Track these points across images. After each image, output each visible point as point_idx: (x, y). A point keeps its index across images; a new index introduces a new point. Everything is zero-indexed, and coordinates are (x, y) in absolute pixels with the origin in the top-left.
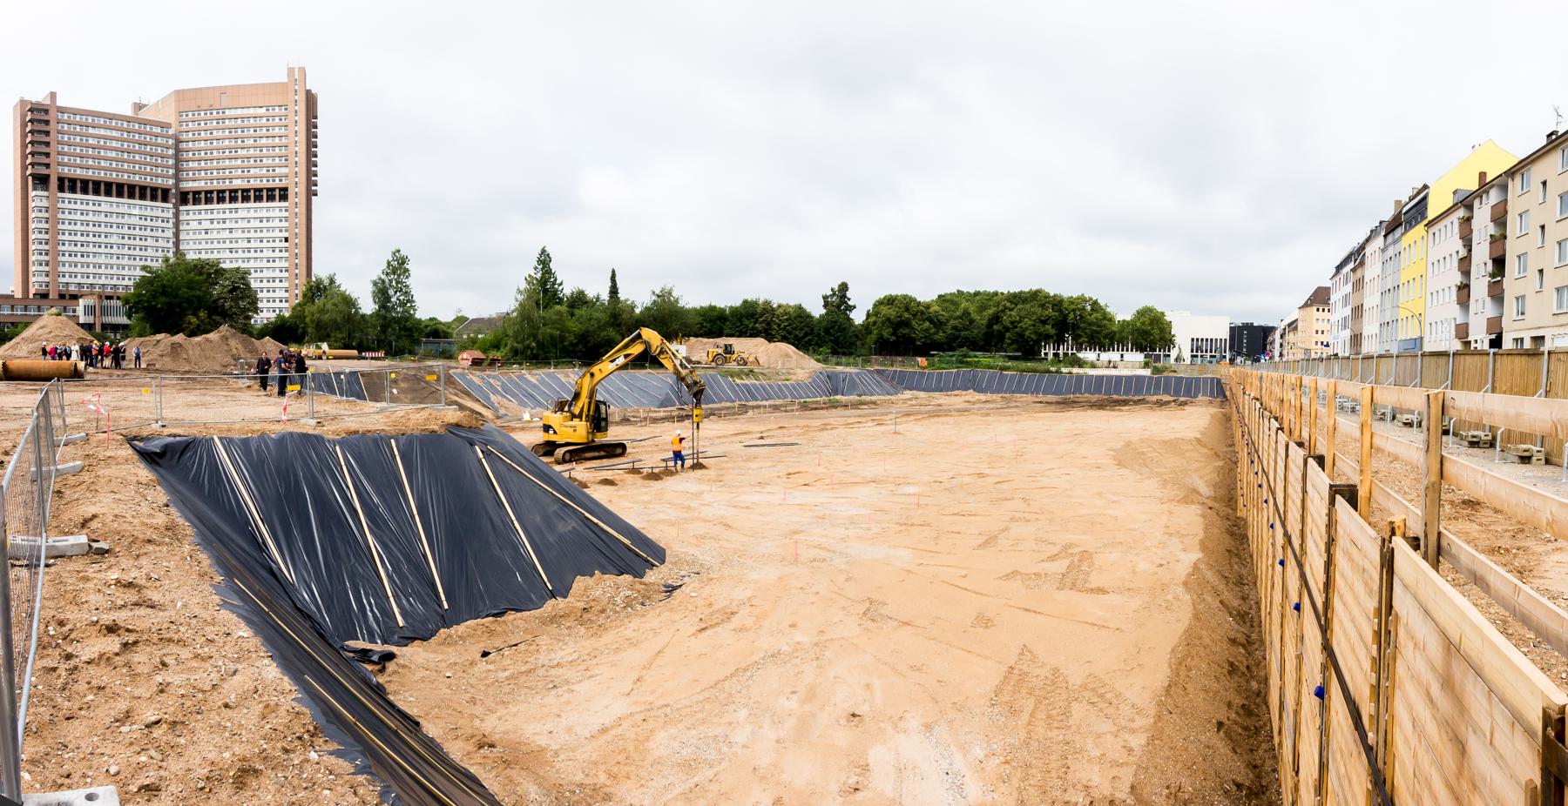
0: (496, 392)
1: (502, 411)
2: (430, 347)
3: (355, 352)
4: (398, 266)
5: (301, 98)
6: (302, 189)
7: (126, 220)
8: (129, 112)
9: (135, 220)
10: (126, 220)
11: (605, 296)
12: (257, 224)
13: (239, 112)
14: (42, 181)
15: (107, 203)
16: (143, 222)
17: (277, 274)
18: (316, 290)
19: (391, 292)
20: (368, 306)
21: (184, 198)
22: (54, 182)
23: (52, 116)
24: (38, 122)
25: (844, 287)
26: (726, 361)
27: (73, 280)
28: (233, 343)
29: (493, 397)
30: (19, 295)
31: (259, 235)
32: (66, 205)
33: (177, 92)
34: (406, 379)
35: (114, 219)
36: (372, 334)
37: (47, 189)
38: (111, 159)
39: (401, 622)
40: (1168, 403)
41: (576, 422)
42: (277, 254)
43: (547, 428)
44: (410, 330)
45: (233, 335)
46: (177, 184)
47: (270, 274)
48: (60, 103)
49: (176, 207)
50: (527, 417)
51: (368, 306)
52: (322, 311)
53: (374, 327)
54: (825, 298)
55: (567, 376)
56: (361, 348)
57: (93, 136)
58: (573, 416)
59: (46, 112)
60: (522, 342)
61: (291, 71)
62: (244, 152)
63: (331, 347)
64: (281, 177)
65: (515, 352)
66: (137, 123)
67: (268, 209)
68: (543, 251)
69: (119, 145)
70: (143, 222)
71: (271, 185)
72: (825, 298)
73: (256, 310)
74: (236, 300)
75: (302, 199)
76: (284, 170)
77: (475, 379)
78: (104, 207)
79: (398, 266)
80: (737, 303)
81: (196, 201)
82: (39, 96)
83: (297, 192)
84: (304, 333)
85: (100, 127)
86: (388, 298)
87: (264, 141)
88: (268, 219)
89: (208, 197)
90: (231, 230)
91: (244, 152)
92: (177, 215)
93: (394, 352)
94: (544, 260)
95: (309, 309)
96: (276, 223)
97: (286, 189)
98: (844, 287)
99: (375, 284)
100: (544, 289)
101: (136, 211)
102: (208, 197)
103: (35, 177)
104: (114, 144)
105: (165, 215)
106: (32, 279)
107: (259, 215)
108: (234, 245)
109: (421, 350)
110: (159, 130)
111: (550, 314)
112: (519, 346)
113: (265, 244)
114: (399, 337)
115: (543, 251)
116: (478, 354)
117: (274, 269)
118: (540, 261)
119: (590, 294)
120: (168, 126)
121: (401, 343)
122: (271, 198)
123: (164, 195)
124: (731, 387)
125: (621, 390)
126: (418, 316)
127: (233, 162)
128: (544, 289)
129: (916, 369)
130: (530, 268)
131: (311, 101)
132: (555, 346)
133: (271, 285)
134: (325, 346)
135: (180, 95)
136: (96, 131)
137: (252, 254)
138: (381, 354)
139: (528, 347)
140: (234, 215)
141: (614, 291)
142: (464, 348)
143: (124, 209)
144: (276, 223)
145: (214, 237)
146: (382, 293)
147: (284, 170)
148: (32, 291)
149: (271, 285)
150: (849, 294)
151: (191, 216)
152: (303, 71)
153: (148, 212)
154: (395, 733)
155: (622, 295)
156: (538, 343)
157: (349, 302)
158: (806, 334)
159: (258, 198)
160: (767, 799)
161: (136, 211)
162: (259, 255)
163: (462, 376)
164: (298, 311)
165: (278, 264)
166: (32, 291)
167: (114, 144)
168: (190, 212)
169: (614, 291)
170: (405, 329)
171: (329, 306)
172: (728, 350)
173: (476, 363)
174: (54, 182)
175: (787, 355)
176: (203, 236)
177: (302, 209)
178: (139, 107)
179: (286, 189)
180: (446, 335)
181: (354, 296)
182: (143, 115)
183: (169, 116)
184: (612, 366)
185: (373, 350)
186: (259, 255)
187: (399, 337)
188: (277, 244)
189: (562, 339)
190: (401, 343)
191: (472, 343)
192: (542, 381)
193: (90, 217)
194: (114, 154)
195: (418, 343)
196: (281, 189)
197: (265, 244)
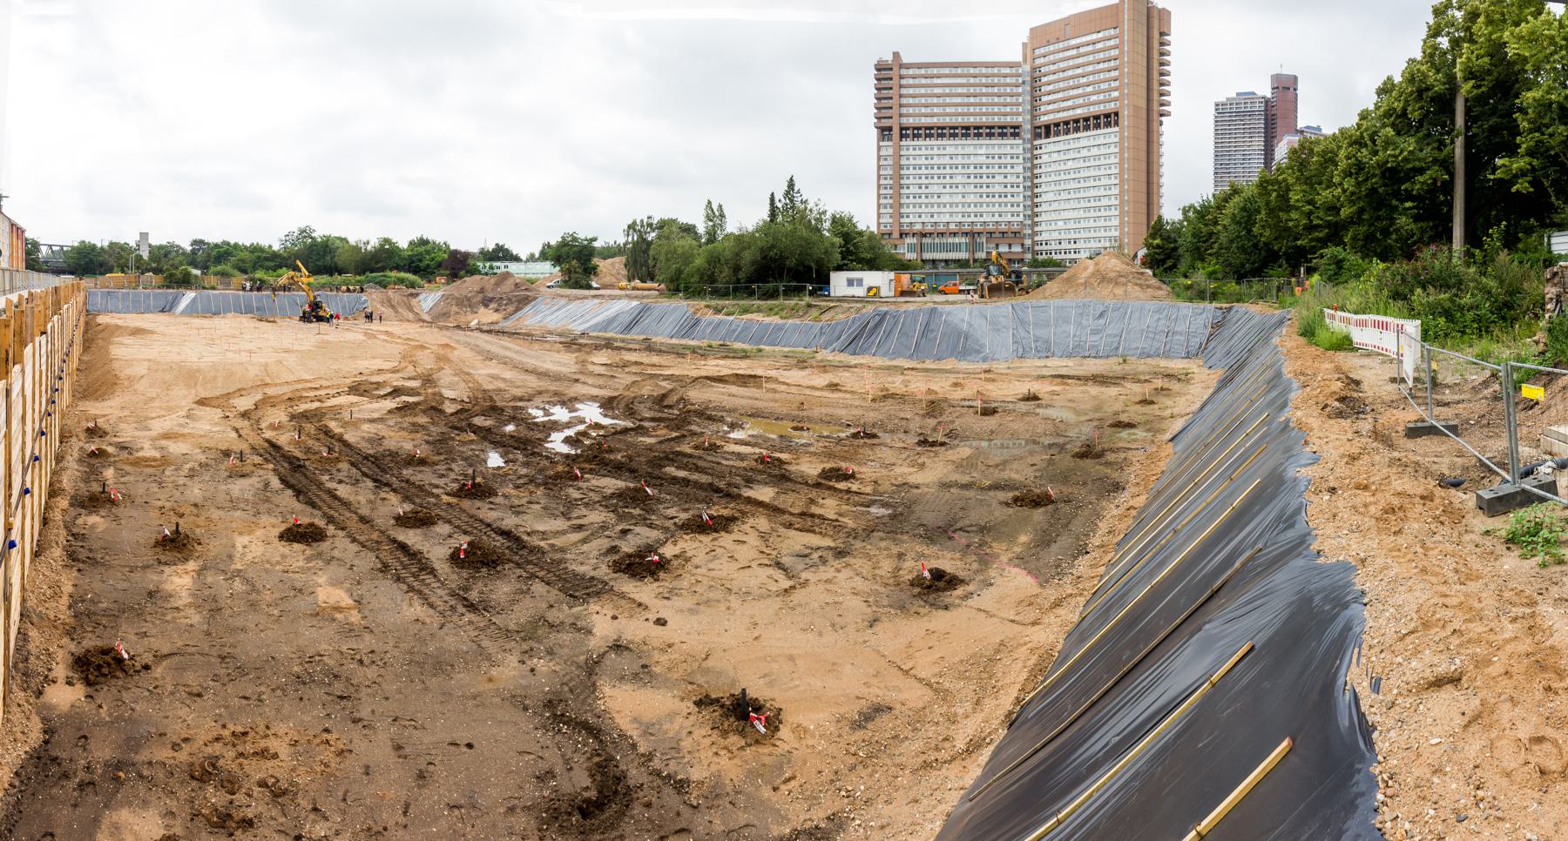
7: (973, 160)
9: (982, 159)
10: (973, 160)
15: (952, 146)
16: (990, 161)
24: (888, 75)
27: (979, 219)
32: (911, 152)
35: (959, 160)
39: (1285, 743)
40: (372, 374)
69: (1013, 80)
70: (990, 161)
78: (950, 150)
80: (218, 240)
89: (929, 132)
102: (929, 132)
105: (1015, 151)
123: (1015, 131)
143: (971, 150)
154: (1059, 822)
160: (513, 760)
168: (1050, 148)
174: (896, 131)
193: (936, 161)
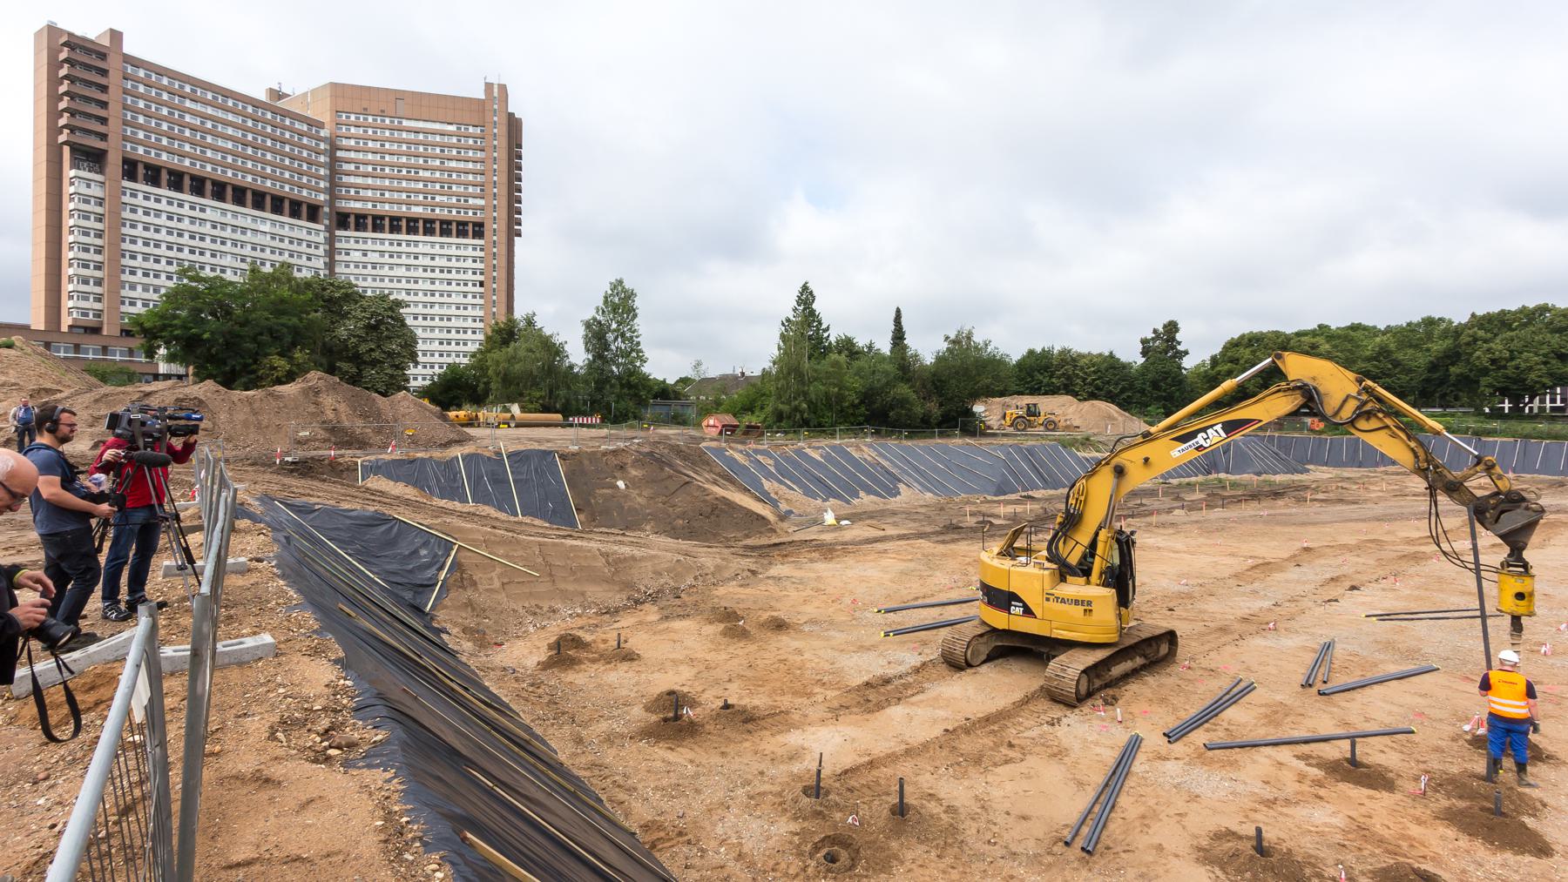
0: (769, 475)
1: (783, 507)
2: (658, 410)
3: (559, 417)
4: (621, 304)
5: (501, 130)
6: (501, 226)
8: (262, 96)
11: (885, 346)
12: (443, 262)
13: (421, 125)
14: (92, 158)
17: (469, 323)
18: (505, 334)
19: (610, 337)
20: (577, 355)
21: (342, 220)
22: (114, 162)
23: (113, 64)
25: (1172, 328)
26: (1030, 425)
28: (328, 401)
29: (767, 485)
30: (39, 323)
31: (445, 275)
33: (334, 86)
34: (638, 463)
36: (583, 393)
37: (101, 172)
38: (225, 151)
41: (1074, 588)
42: (469, 299)
43: (1001, 598)
44: (635, 387)
45: (333, 388)
46: (331, 203)
47: (461, 323)
48: (128, 48)
49: (329, 229)
50: (830, 518)
51: (577, 355)
52: (512, 359)
53: (587, 382)
54: (1144, 342)
55: (858, 448)
56: (567, 411)
57: (194, 113)
58: (1064, 571)
59: (103, 56)
60: (789, 403)
61: (489, 87)
62: (427, 174)
63: (523, 409)
64: (475, 209)
65: (779, 416)
66: (272, 111)
67: (458, 246)
68: (805, 288)
71: (462, 217)
72: (1144, 342)
73: (413, 357)
74: (380, 341)
75: (501, 238)
76: (481, 202)
77: (737, 456)
79: (621, 304)
81: (360, 226)
82: (90, 28)
83: (496, 227)
84: (487, 392)
85: (206, 103)
86: (606, 347)
87: (453, 164)
88: (458, 258)
90: (408, 267)
91: (427, 174)
92: (331, 241)
93: (615, 418)
94: (806, 297)
95: (496, 355)
96: (469, 263)
97: (481, 225)
98: (1172, 328)
99: (588, 325)
100: (805, 328)
101: (266, 227)
103: (76, 149)
104: (230, 131)
105: (312, 238)
106: (67, 304)
107: (445, 251)
108: (412, 286)
109: (649, 413)
110: (305, 128)
111: (824, 366)
112: (785, 408)
113: (453, 287)
114: (620, 397)
115: (805, 288)
116: (729, 419)
117: (465, 318)
118: (800, 301)
119: (861, 342)
120: (320, 125)
121: (622, 404)
122: (462, 233)
123: (313, 213)
124: (1079, 461)
125: (935, 469)
126: (646, 369)
127: (413, 185)
128: (805, 328)
129: (1305, 434)
130: (787, 306)
131: (514, 127)
132: (830, 407)
133: (461, 336)
134: (515, 409)
135: (339, 91)
136: (198, 107)
137: (437, 298)
138: (596, 419)
139: (796, 409)
140: (412, 249)
141: (899, 336)
142: (705, 411)
144: (469, 263)
145: (372, 265)
146: (597, 336)
147: (481, 202)
148: (66, 322)
149: (461, 336)
150: (1178, 337)
151: (352, 244)
152: (503, 88)
153: (286, 231)
155: (910, 341)
156: (810, 403)
157: (552, 350)
158: (1123, 391)
159: (445, 232)
161: (266, 227)
162: (445, 299)
163: (719, 452)
164: (480, 358)
165: (470, 312)
166: (66, 322)
167: (230, 131)
169: (899, 336)
170: (629, 385)
171: (522, 353)
172: (1032, 411)
173: (730, 429)
174: (114, 162)
175: (1111, 418)
176: (369, 270)
177: (501, 250)
178: (277, 95)
179: (481, 225)
180: (677, 395)
181: (558, 340)
182: (280, 104)
183: (321, 112)
184: (1179, 453)
185: (585, 414)
186: (445, 299)
187: (620, 397)
188: (470, 288)
189: (840, 398)
190: (622, 404)
191: (716, 407)
192: (827, 457)
194: (230, 145)
195: (642, 403)
196: (475, 224)
197: (453, 287)
